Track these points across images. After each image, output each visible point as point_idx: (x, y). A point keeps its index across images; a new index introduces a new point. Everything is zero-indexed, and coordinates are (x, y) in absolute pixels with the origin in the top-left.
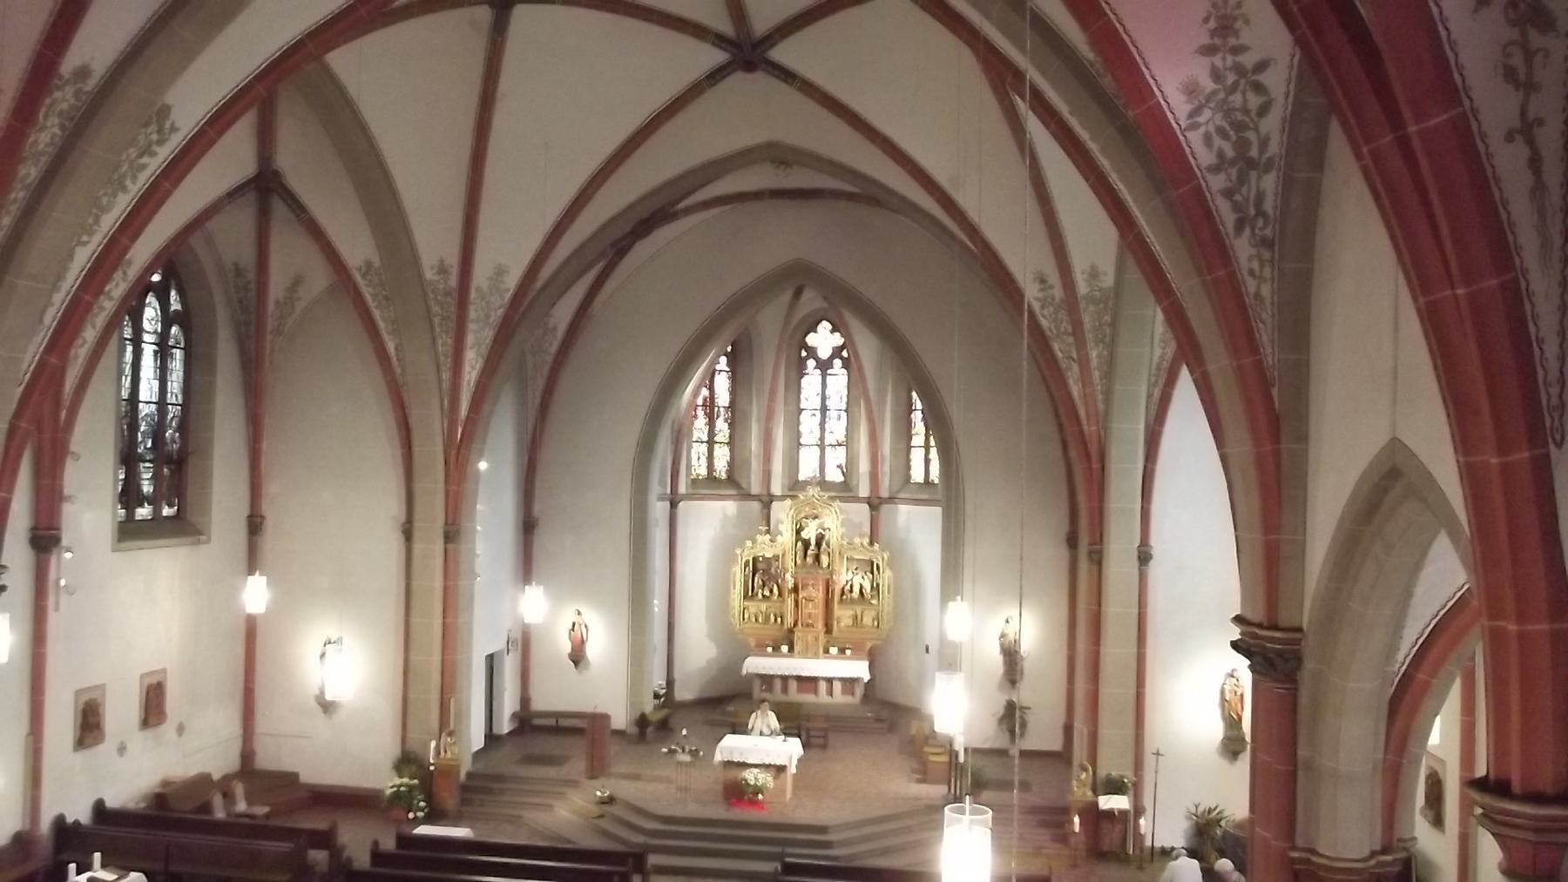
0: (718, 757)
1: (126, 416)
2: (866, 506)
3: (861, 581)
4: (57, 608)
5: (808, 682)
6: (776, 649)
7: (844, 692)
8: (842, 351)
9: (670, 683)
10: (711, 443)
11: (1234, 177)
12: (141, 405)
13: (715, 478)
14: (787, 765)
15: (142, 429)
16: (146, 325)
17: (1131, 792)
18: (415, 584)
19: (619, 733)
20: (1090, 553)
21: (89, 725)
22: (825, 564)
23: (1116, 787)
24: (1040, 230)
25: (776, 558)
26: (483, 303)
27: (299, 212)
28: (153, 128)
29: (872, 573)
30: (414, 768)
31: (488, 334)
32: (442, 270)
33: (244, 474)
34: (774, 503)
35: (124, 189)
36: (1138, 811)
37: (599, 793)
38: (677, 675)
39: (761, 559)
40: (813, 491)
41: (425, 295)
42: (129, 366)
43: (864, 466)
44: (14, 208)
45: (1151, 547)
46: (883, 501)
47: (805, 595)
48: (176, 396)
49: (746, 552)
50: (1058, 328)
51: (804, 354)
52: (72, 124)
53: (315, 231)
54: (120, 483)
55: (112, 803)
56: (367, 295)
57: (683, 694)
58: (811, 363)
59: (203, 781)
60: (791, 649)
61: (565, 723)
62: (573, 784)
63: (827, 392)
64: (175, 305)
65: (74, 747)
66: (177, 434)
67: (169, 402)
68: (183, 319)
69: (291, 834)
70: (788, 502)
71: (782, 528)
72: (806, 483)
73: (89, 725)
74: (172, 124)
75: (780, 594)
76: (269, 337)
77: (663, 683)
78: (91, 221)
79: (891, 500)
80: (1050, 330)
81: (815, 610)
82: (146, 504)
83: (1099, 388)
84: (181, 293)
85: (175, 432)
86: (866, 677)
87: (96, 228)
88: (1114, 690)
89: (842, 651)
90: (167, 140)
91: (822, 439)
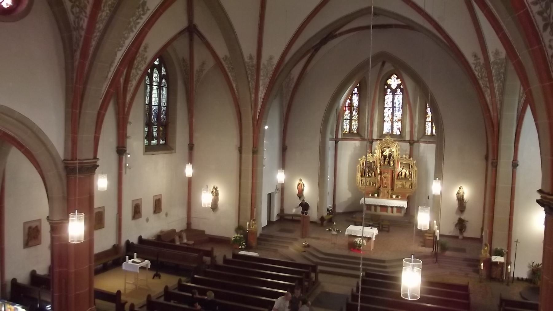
0: (347, 233)
1: (148, 110)
2: (408, 144)
3: (405, 171)
4: (126, 173)
5: (385, 208)
6: (373, 195)
7: (398, 212)
8: (401, 86)
9: (334, 206)
10: (351, 120)
11: (544, 6)
12: (153, 106)
13: (352, 132)
14: (372, 237)
15: (153, 114)
16: (154, 80)
17: (506, 256)
18: (243, 168)
19: (312, 222)
20: (492, 163)
21: (137, 212)
22: (392, 165)
23: (499, 253)
24: (475, 35)
25: (374, 162)
26: (265, 70)
27: (202, 39)
28: (141, 9)
29: (410, 169)
30: (242, 231)
31: (267, 81)
32: (251, 58)
33: (187, 130)
34: (374, 142)
35: (133, 31)
36: (508, 263)
37: (304, 243)
38: (337, 203)
39: (368, 162)
40: (388, 138)
41: (245, 66)
42: (148, 93)
43: (408, 129)
44: (96, 39)
45: (518, 161)
46: (415, 142)
47: (384, 176)
48: (164, 103)
49: (363, 160)
50: (481, 75)
51: (386, 87)
52: (113, 9)
53: (208, 46)
54: (146, 132)
55: (144, 237)
56: (226, 67)
57: (339, 210)
58: (389, 90)
59: (174, 231)
60: (378, 196)
61: (295, 218)
62: (296, 239)
63: (395, 101)
64: (163, 73)
65: (132, 219)
66: (165, 116)
67: (162, 105)
68: (166, 77)
69: (198, 251)
70: (379, 142)
71: (376, 151)
72: (386, 135)
73: (137, 212)
74: (147, 8)
75: (375, 176)
76: (195, 83)
77: (331, 205)
78: (122, 42)
79: (418, 142)
80: (479, 76)
81: (388, 182)
82: (155, 140)
83: (498, 98)
84: (165, 68)
85: (164, 115)
86: (406, 206)
87: (124, 45)
88: (500, 215)
89: (397, 197)
90: (146, 13)
91: (392, 118)
